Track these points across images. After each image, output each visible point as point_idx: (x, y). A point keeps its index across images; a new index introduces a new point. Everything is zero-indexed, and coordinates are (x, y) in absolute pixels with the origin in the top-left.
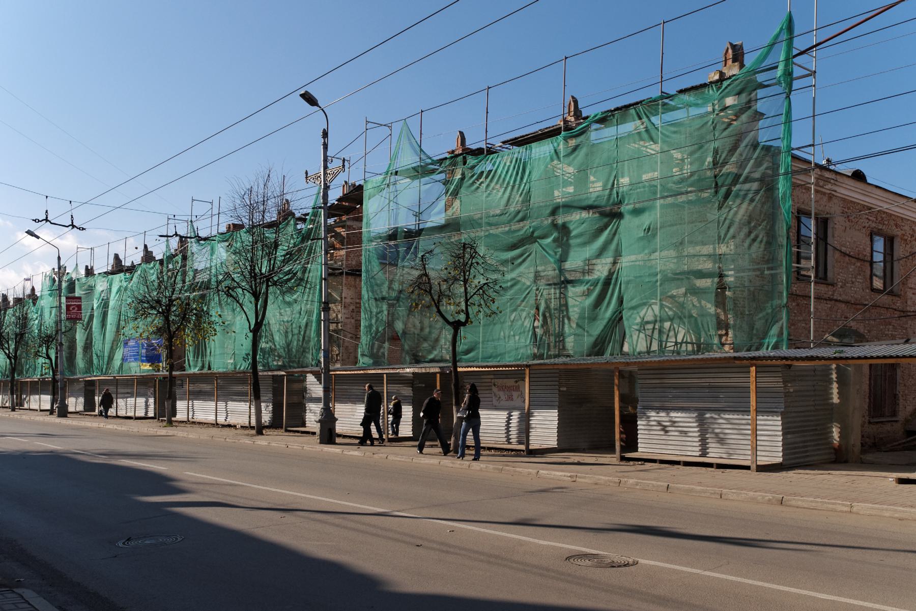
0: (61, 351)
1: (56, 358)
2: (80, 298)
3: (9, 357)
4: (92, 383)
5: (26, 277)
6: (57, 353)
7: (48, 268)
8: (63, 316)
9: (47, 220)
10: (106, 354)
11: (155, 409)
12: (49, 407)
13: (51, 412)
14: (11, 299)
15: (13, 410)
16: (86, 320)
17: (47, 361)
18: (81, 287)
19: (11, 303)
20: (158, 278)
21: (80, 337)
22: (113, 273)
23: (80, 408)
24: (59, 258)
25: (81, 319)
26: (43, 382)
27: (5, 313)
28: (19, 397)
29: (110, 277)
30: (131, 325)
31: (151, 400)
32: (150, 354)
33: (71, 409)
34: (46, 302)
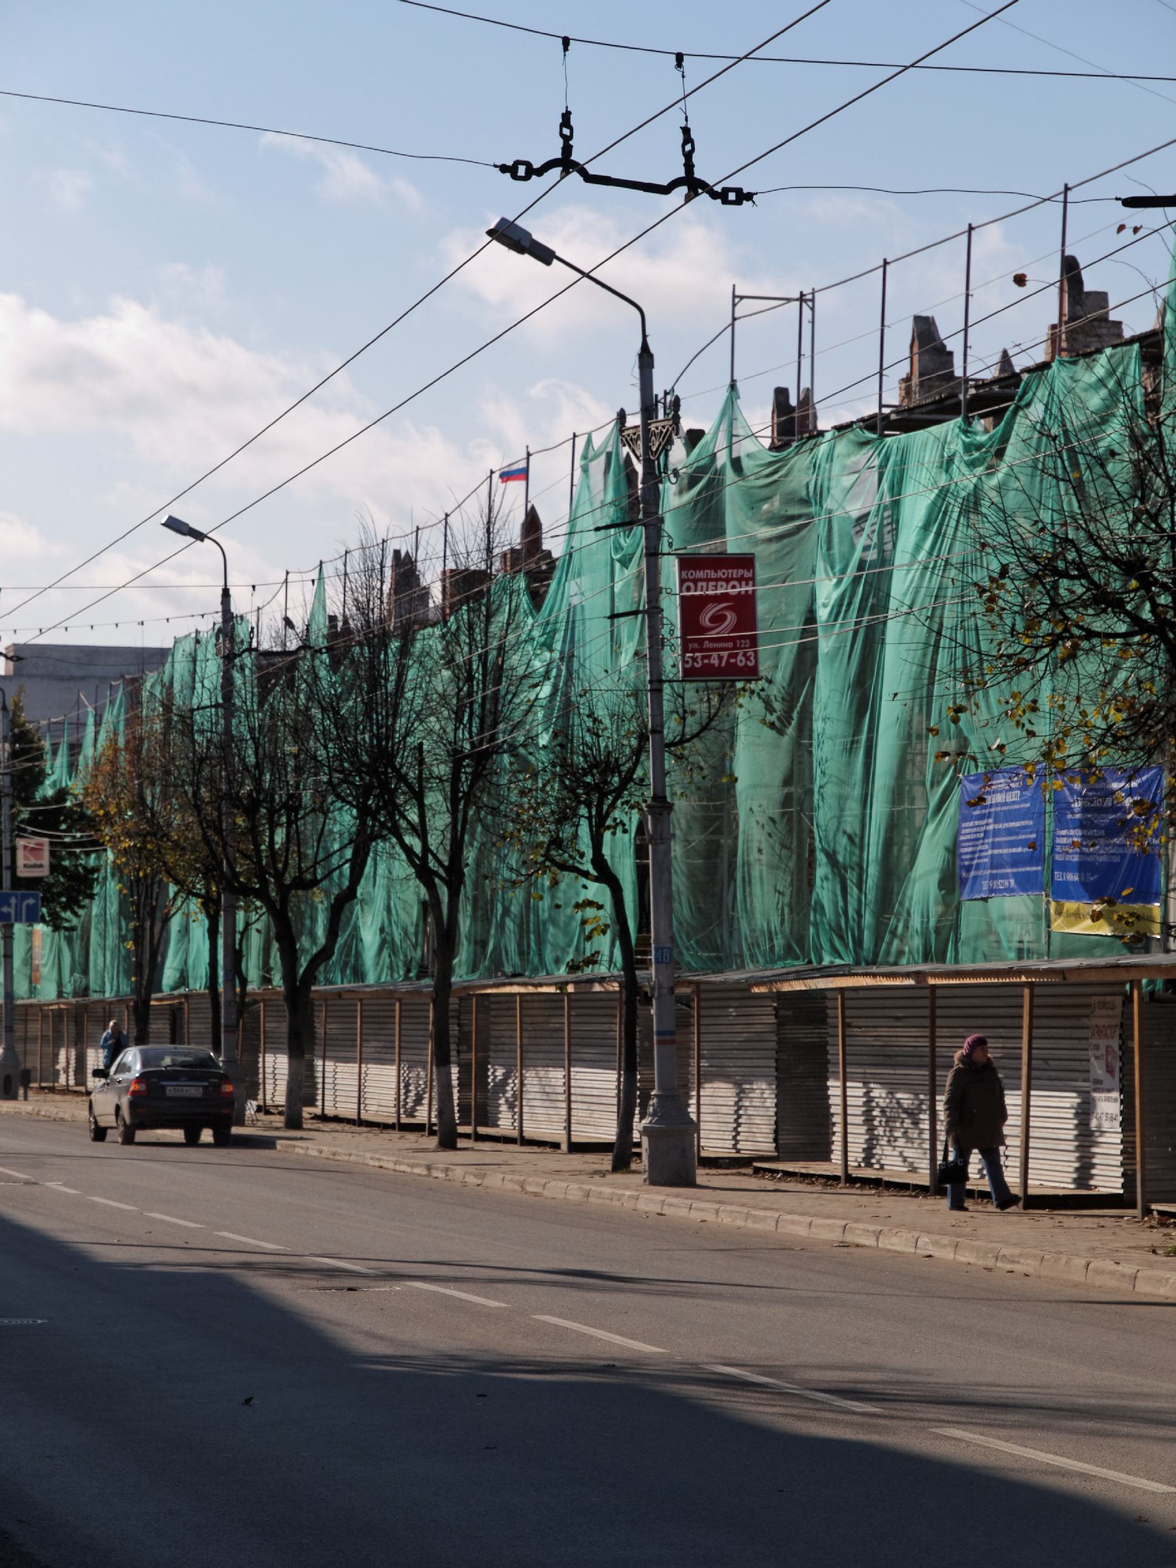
0: (662, 838)
1: (642, 873)
2: (746, 562)
3: (424, 874)
4: (808, 1010)
5: (497, 463)
6: (640, 852)
7: (596, 408)
8: (672, 659)
9: (566, 163)
10: (873, 852)
11: (1127, 1152)
12: (608, 1132)
13: (621, 1154)
14: (431, 577)
15: (448, 1142)
16: (781, 677)
17: (596, 891)
18: (753, 502)
19: (436, 596)
20: (1136, 441)
21: (755, 761)
22: (908, 420)
23: (759, 1138)
24: (646, 358)
25: (751, 673)
26: (583, 1002)
27: (404, 652)
28: (474, 1078)
29: (895, 440)
30: (993, 700)
31: (1108, 1106)
32: (1101, 853)
33: (714, 1139)
34: (594, 583)
